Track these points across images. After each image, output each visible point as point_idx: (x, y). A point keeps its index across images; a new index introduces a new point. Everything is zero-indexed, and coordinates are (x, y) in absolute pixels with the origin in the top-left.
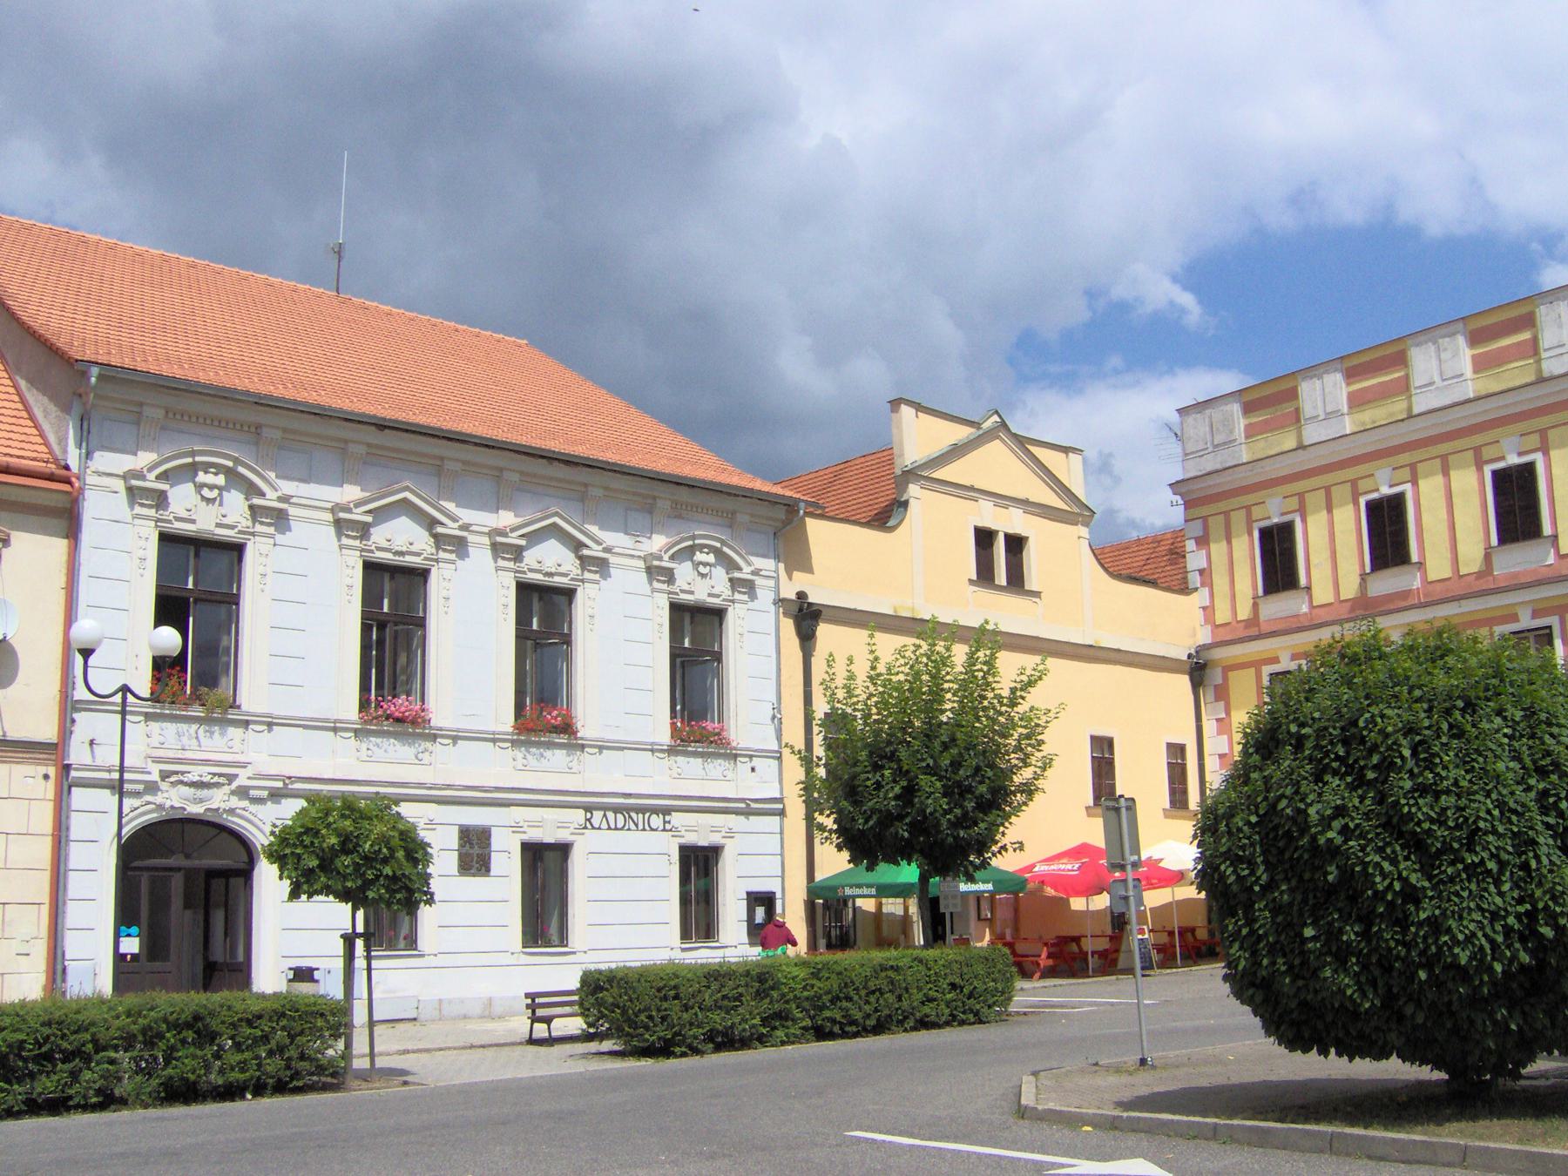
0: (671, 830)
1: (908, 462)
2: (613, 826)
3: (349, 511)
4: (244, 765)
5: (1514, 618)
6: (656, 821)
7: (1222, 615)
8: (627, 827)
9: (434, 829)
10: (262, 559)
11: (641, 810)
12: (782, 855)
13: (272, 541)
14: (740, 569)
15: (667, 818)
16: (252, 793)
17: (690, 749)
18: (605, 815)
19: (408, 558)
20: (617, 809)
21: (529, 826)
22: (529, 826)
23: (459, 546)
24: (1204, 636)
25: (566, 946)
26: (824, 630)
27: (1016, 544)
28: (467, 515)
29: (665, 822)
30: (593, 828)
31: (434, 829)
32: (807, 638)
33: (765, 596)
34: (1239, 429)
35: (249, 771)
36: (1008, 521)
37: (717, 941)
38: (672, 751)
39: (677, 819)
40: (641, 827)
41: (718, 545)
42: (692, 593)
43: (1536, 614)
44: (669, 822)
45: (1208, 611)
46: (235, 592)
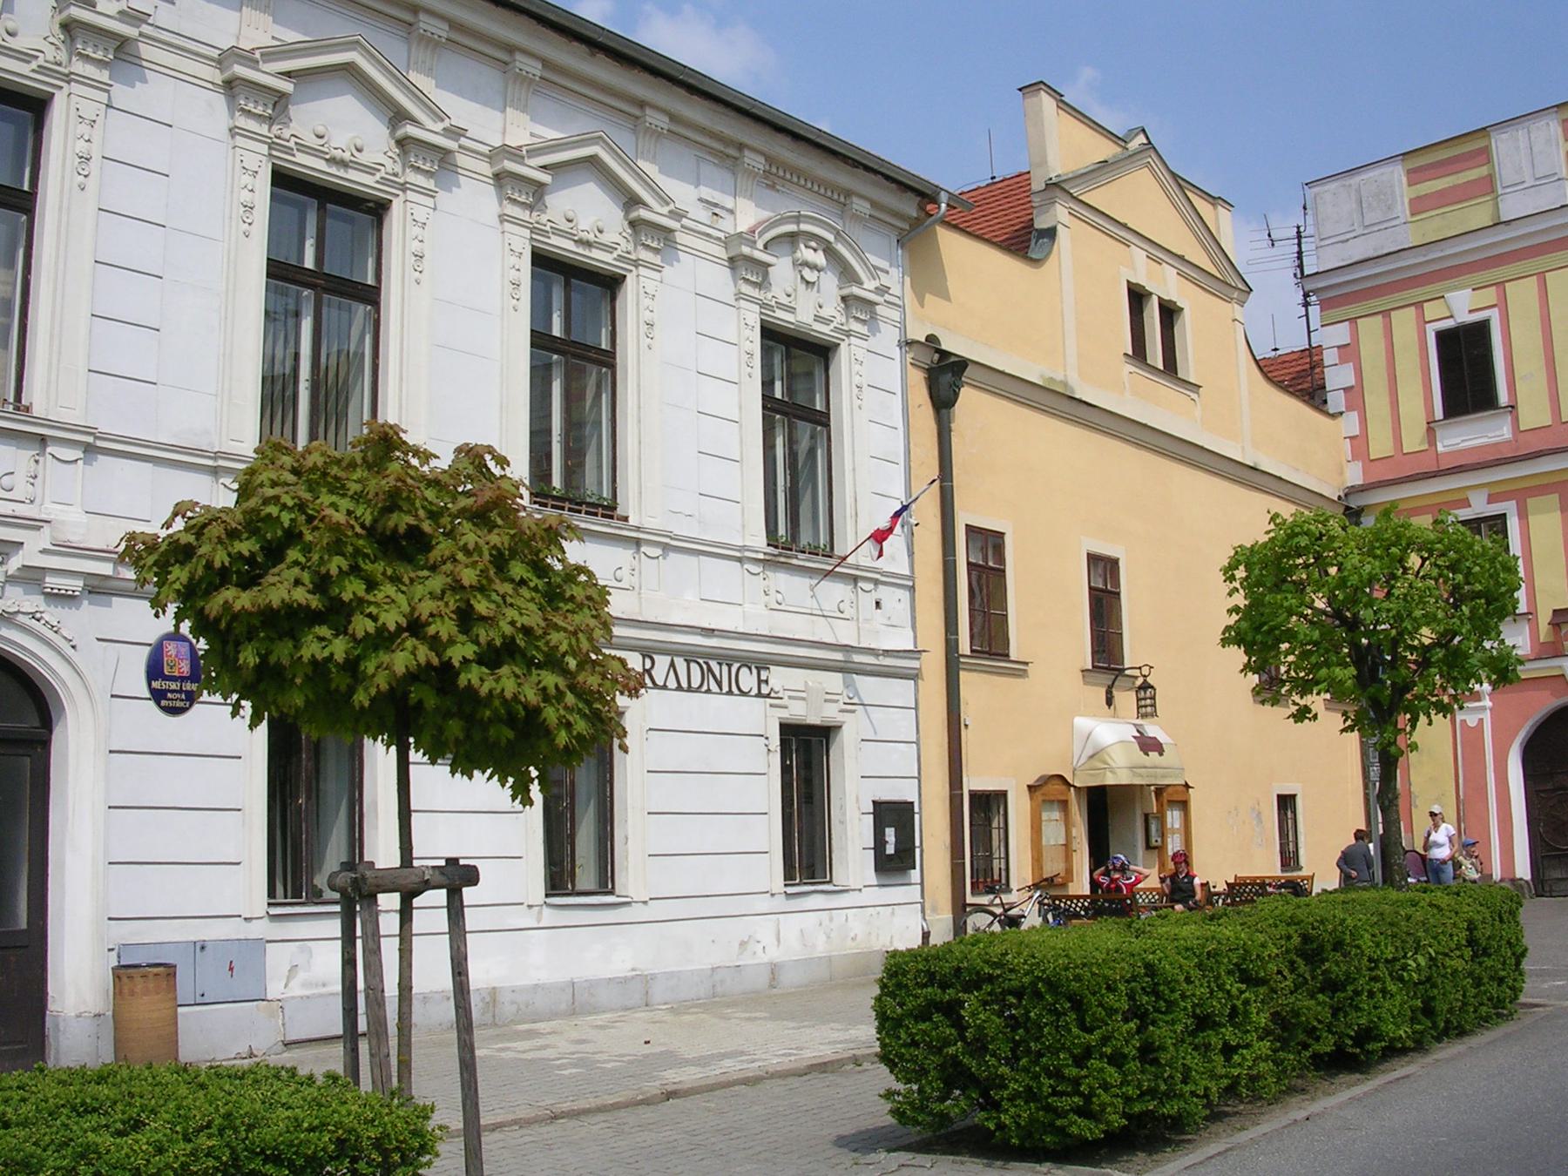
0: (768, 696)
1: (1053, 175)
2: (684, 684)
3: (253, 63)
4: (35, 524)
5: (1466, 503)
6: (748, 680)
7: (1380, 445)
8: (705, 688)
9: (853, 711)
10: (84, 129)
11: (726, 658)
12: (917, 743)
13: (103, 97)
14: (859, 282)
15: (764, 675)
16: (51, 581)
17: (794, 561)
18: (672, 665)
19: (353, 175)
20: (691, 656)
21: (790, 697)
22: (790, 697)
23: (442, 162)
24: (1354, 475)
25: (612, 893)
26: (969, 400)
27: (1169, 312)
28: (460, 110)
29: (760, 681)
30: (655, 686)
31: (853, 711)
32: (943, 403)
33: (888, 338)
34: (1403, 203)
35: (43, 539)
36: (1165, 284)
37: (830, 882)
38: (768, 563)
39: (778, 678)
40: (726, 689)
41: (831, 238)
42: (792, 310)
43: (1492, 499)
44: (766, 682)
45: (1359, 444)
46: (26, 188)
